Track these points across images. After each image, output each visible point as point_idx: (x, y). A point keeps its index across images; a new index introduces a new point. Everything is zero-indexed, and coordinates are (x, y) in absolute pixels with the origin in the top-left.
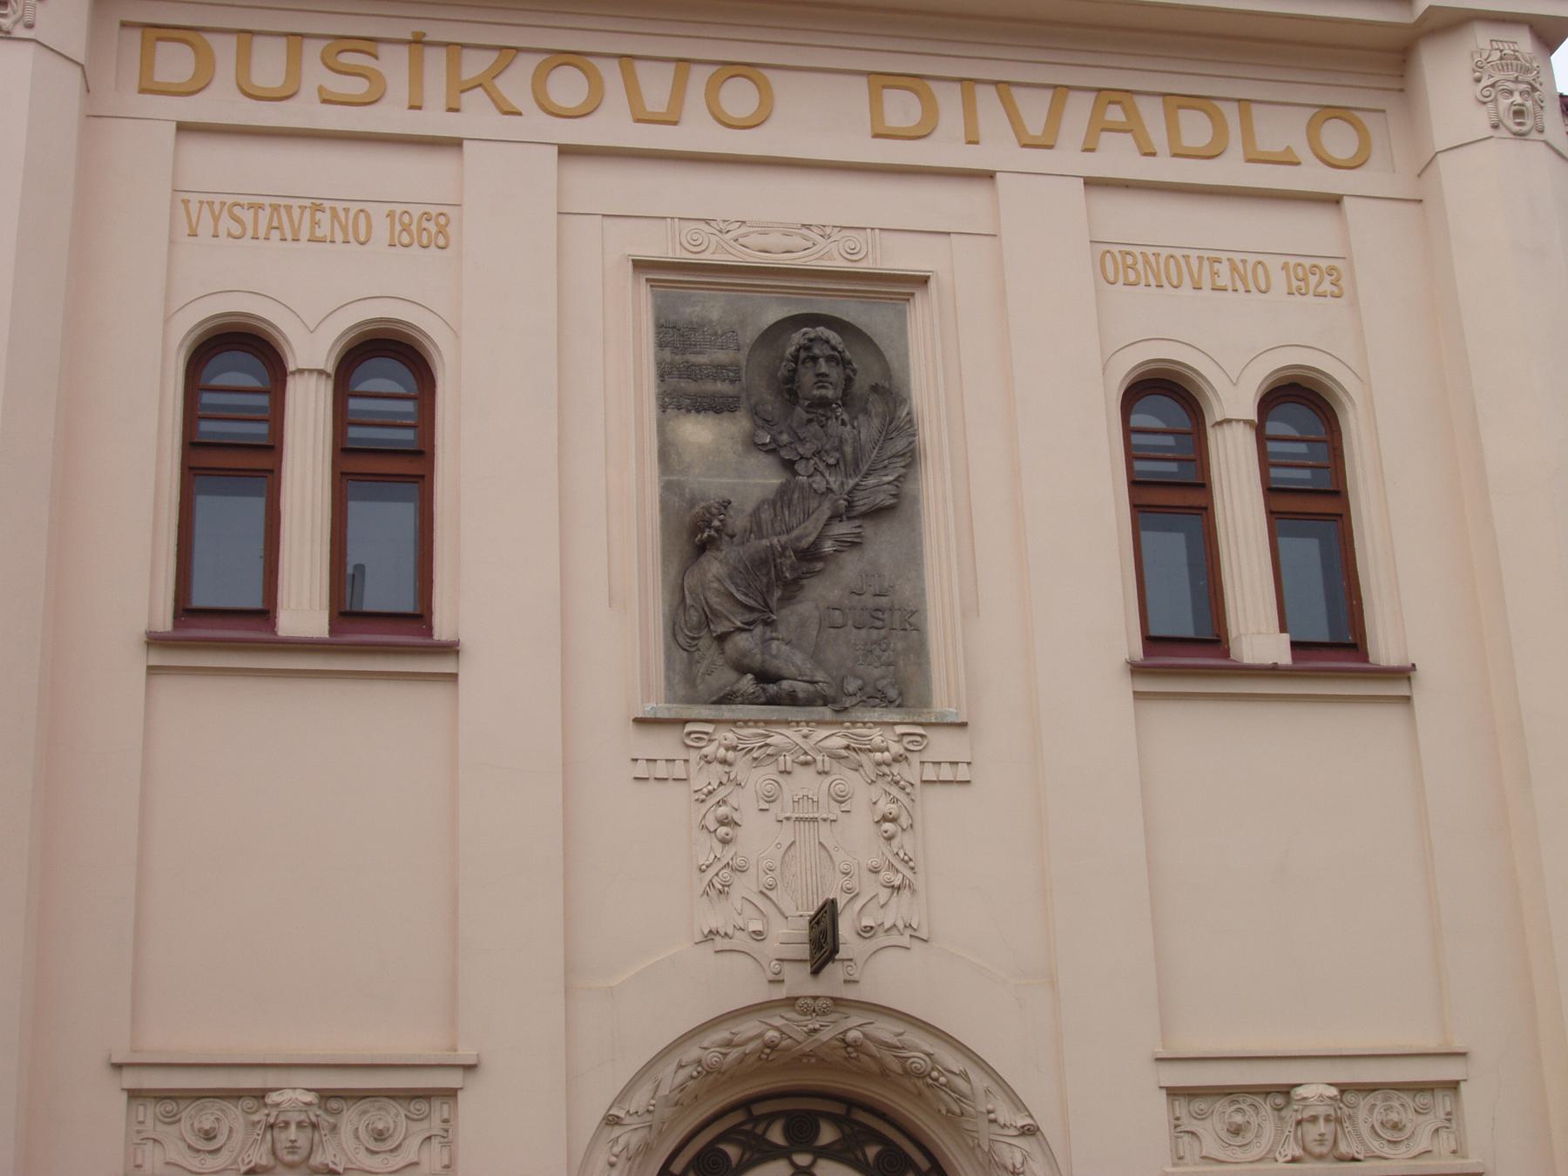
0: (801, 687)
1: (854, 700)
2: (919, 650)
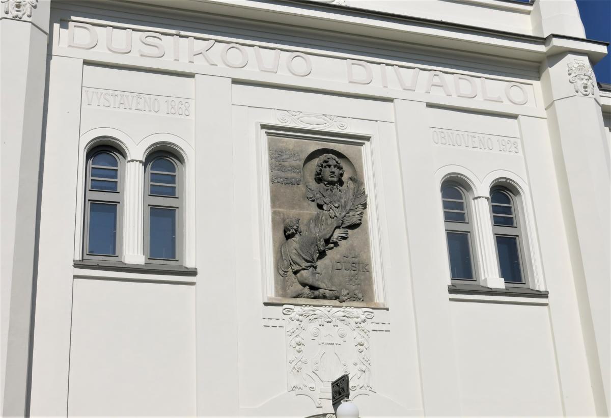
0: (328, 293)
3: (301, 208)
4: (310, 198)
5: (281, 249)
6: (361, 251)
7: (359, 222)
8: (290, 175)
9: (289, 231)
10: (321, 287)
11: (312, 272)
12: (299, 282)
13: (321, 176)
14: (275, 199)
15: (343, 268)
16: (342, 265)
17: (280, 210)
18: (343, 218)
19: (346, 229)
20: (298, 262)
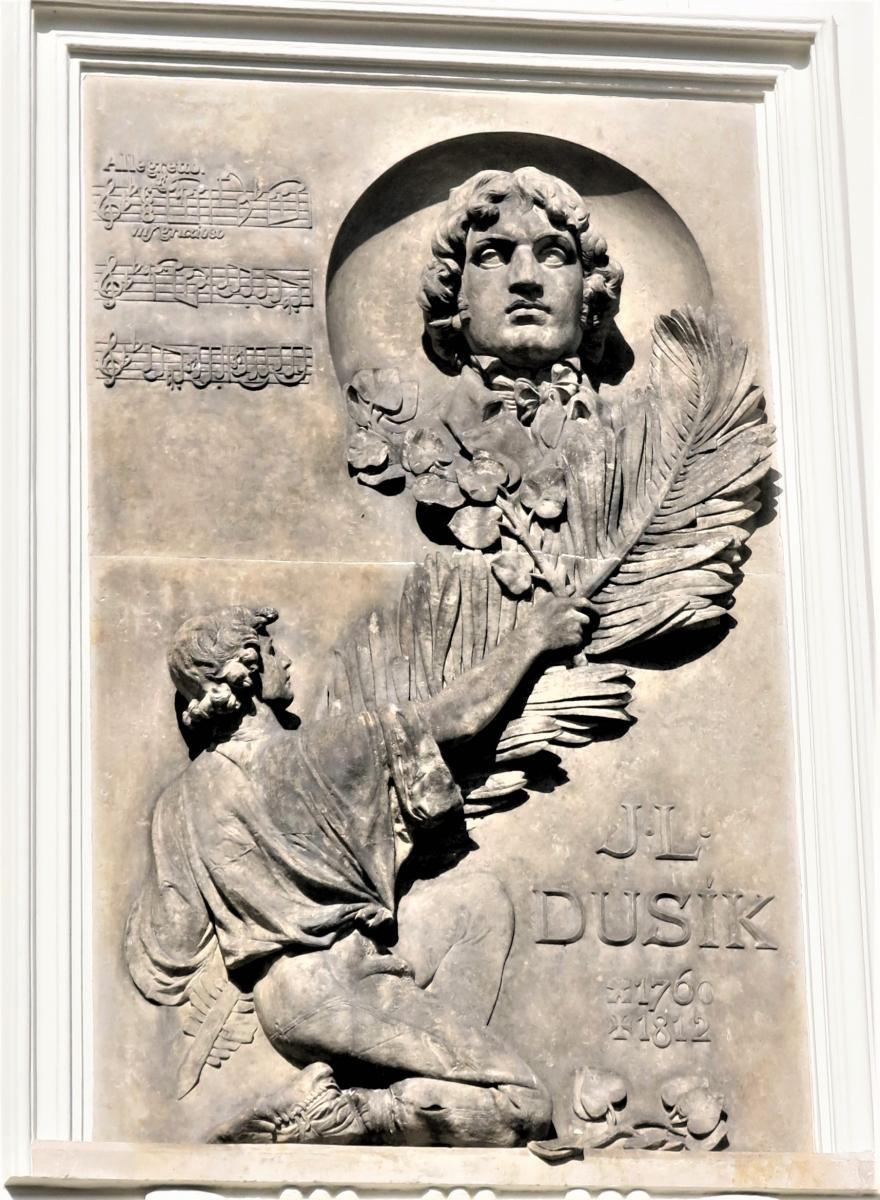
0: (458, 1103)
1: (602, 1130)
2: (777, 1001)
3: (306, 539)
4: (372, 470)
5: (150, 818)
6: (723, 813)
7: (716, 611)
8: (233, 324)
9: (200, 696)
10: (413, 1059)
11: (350, 966)
12: (268, 1033)
13: (456, 321)
14: (121, 490)
15: (594, 930)
16: (583, 909)
17: (160, 559)
18: (598, 590)
19: (616, 669)
20: (253, 901)
